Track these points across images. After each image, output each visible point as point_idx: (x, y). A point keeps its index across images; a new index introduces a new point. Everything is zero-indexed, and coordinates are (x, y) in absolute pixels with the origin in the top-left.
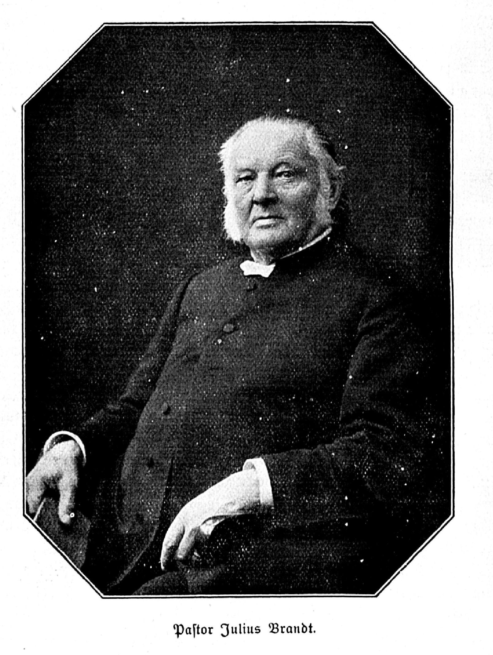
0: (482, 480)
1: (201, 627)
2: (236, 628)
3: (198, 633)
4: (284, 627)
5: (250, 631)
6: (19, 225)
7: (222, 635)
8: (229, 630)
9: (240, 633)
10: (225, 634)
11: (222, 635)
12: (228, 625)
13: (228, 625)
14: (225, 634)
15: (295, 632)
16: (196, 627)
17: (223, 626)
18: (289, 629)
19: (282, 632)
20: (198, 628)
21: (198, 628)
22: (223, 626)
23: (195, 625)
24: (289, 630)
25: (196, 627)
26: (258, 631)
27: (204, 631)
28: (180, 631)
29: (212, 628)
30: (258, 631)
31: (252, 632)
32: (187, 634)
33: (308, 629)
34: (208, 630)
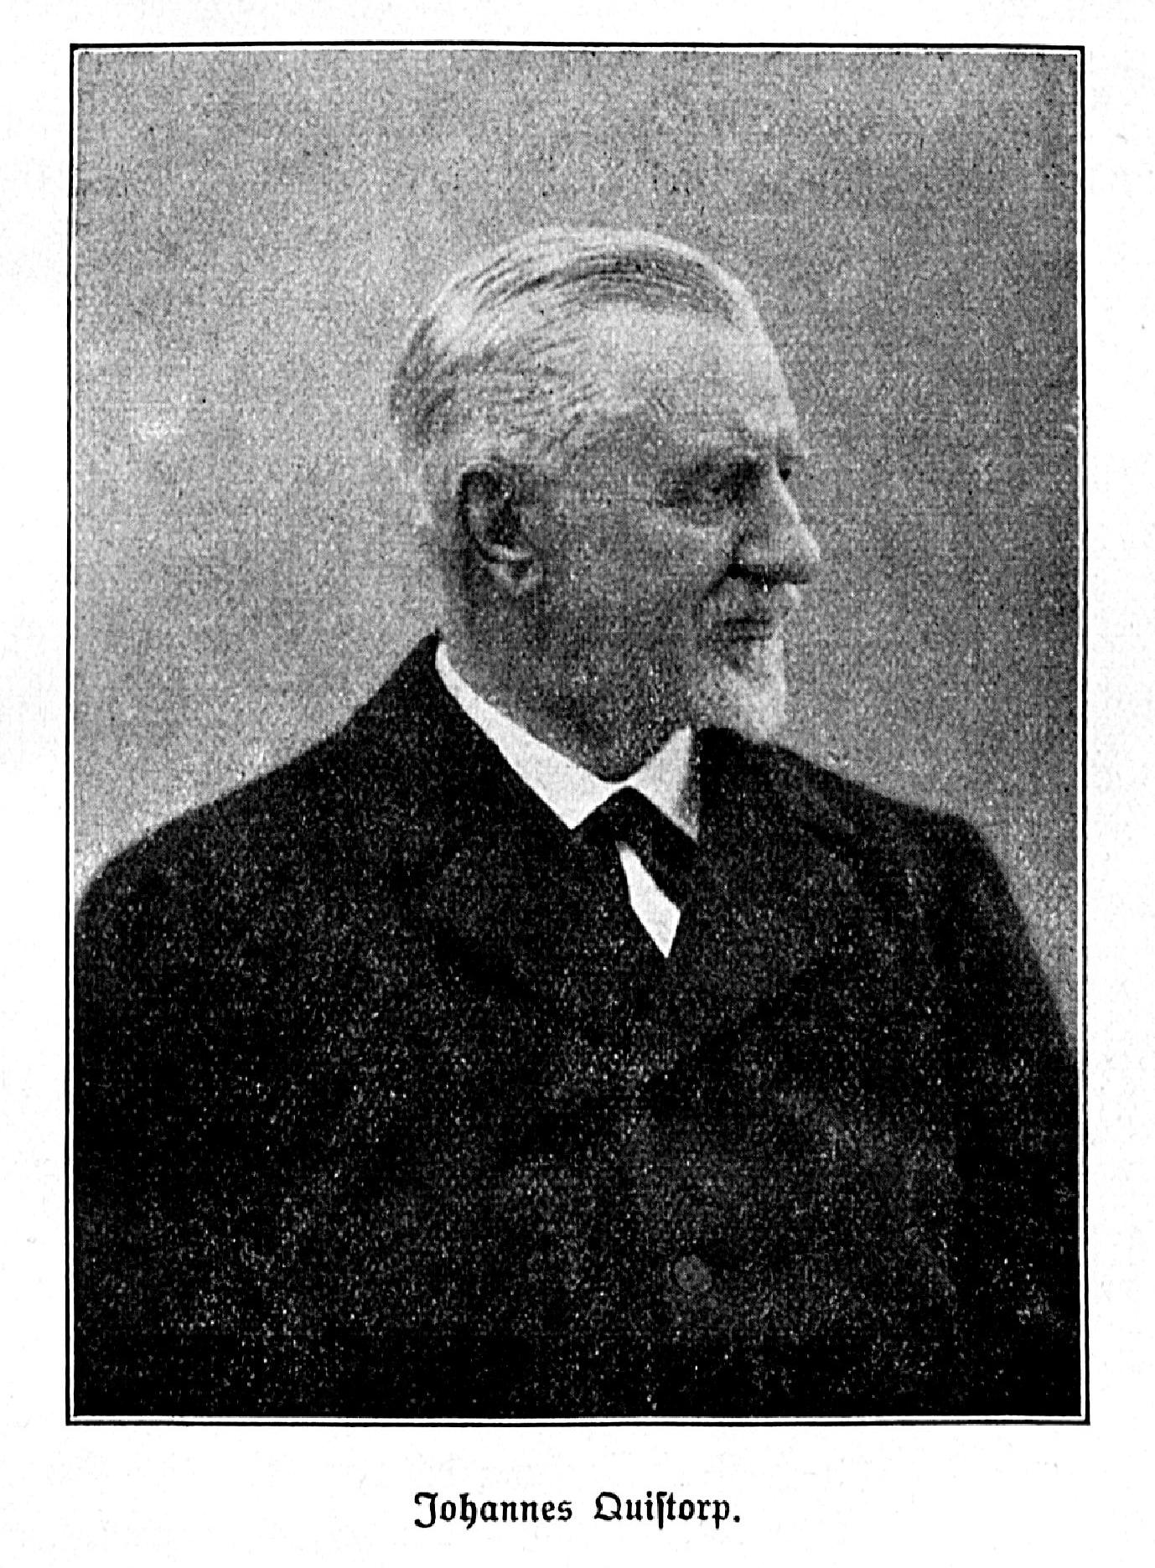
0: (1119, 1118)
1: (678, 1500)
2: (638, 1503)
3: (671, 1517)
4: (708, 1503)
5: (634, 1512)
6: (1094, 765)
7: (418, 1523)
8: (612, 1508)
10: (426, 1520)
11: (418, 1523)
12: (433, 1497)
13: (433, 1497)
14: (426, 1520)
15: (505, 1518)
16: (665, 1499)
17: (421, 1499)
18: (488, 1511)
19: (703, 1517)
20: (671, 1502)
22: (421, 1499)
23: (664, 1494)
24: (488, 1513)
25: (665, 1499)
26: (565, 1514)
27: (687, 1512)
28: (722, 1513)
30: (567, 1514)
32: (485, 1519)
34: (697, 1507)
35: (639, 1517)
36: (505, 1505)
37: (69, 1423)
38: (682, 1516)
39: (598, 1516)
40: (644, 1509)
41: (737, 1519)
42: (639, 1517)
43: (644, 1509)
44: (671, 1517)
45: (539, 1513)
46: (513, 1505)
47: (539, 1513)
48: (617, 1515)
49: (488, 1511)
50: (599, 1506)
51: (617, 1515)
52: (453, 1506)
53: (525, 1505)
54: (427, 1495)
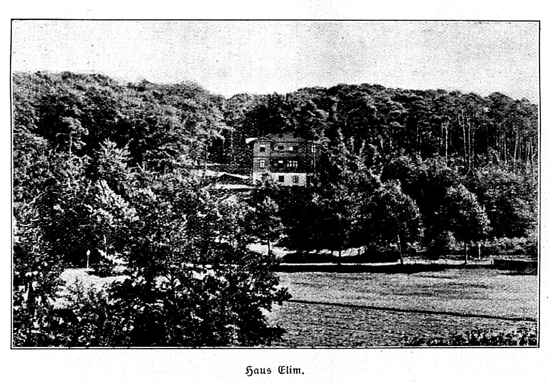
31: (265, 373)
36: (294, 369)
37: (11, 349)
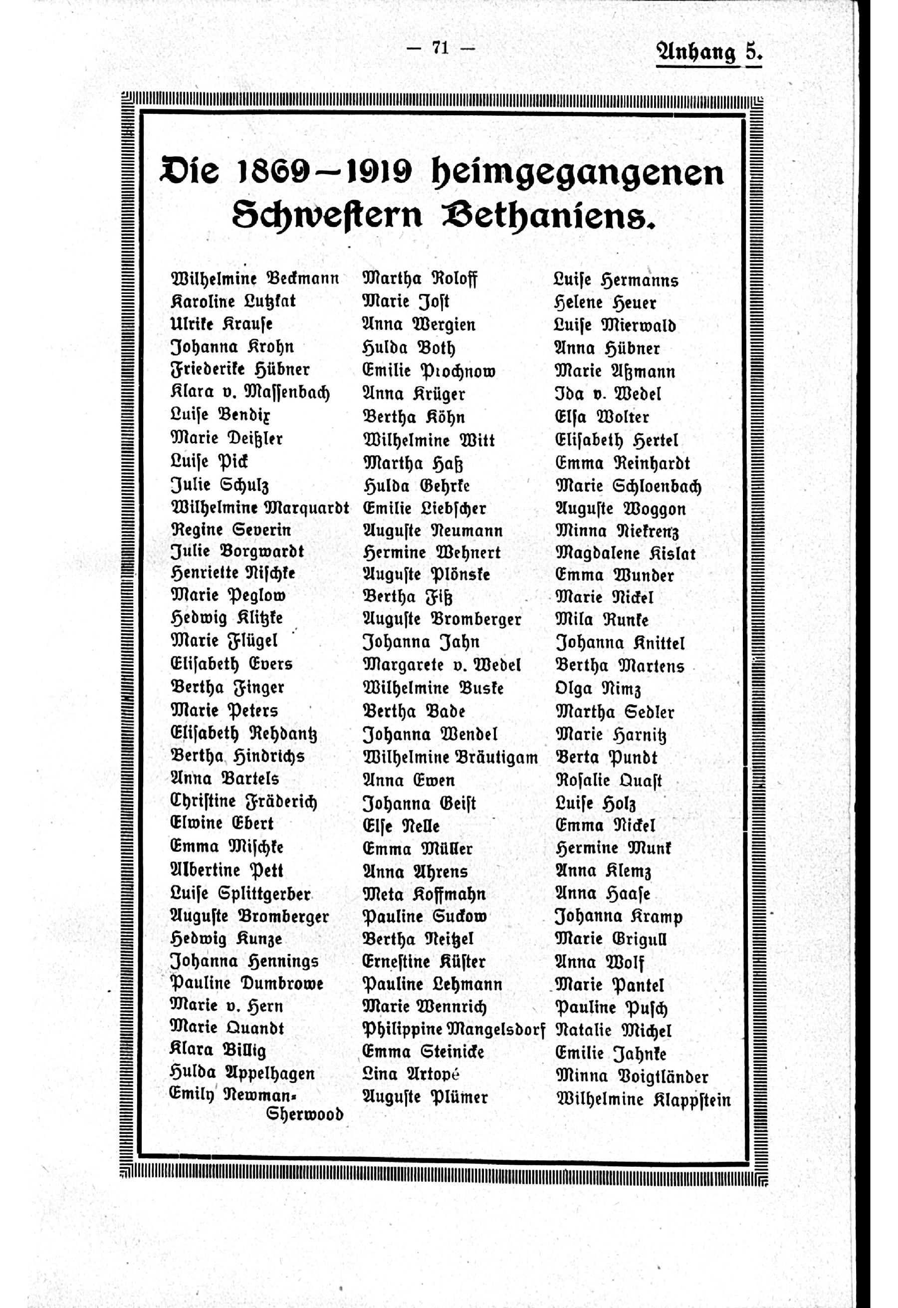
1: (710, 1097)
3: (219, 920)
7: (615, 1060)
9: (217, 805)
13: (371, 798)
16: (402, 958)
21: (228, 570)
25: (402, 958)
29: (484, 960)
30: (731, 54)
33: (640, 1077)
35: (493, 762)
38: (266, 599)
39: (622, 784)
40: (191, 462)
41: (235, 397)
42: (493, 762)
43: (191, 462)
44: (219, 920)
45: (232, 873)
46: (602, 640)
47: (232, 873)
48: (630, 784)
49: (589, 916)
50: (229, 1027)
51: (630, 784)
52: (573, 914)
53: (387, 779)
54: (368, 797)
